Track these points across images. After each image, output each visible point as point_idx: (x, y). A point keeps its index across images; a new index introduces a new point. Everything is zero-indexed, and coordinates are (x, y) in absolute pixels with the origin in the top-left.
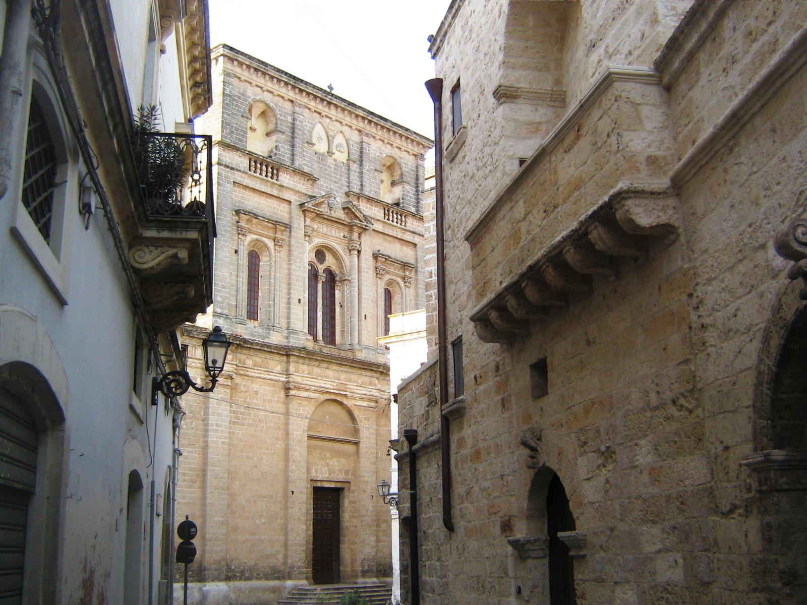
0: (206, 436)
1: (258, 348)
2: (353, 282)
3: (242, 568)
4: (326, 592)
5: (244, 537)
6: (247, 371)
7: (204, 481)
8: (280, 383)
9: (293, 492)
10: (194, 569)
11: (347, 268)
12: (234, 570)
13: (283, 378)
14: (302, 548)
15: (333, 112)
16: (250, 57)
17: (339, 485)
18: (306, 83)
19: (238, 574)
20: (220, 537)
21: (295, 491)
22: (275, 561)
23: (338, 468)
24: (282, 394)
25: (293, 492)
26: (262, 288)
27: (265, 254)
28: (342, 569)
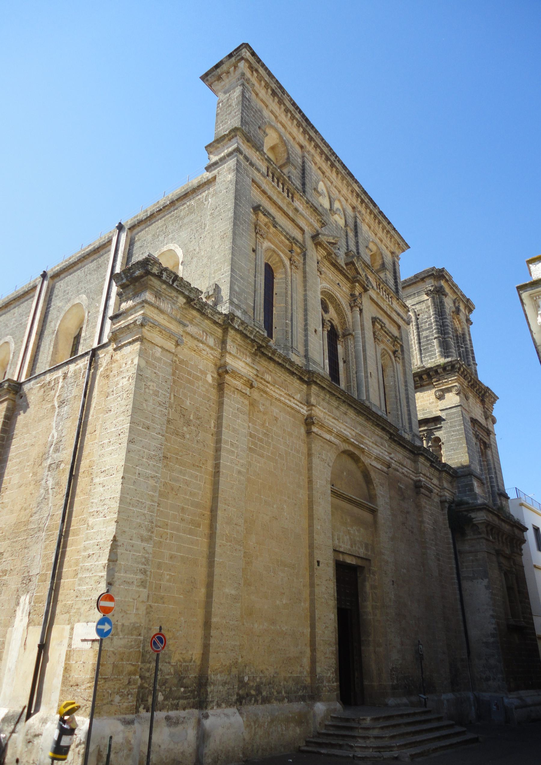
0: (217, 458)
1: (280, 361)
2: (358, 337)
3: (258, 680)
4: (395, 732)
5: (261, 627)
6: (267, 387)
7: (212, 527)
8: (300, 415)
9: (318, 562)
10: (189, 682)
11: (350, 324)
12: (247, 684)
13: (304, 410)
14: (331, 648)
15: (333, 176)
16: (270, 74)
17: (359, 563)
18: (316, 132)
19: (253, 692)
20: (231, 623)
21: (321, 561)
22: (299, 669)
23: (358, 539)
24: (303, 430)
25: (318, 562)
26: (277, 305)
27: (280, 270)
28: (366, 683)
